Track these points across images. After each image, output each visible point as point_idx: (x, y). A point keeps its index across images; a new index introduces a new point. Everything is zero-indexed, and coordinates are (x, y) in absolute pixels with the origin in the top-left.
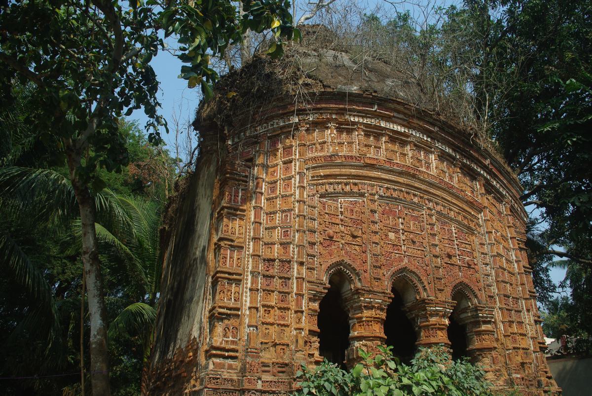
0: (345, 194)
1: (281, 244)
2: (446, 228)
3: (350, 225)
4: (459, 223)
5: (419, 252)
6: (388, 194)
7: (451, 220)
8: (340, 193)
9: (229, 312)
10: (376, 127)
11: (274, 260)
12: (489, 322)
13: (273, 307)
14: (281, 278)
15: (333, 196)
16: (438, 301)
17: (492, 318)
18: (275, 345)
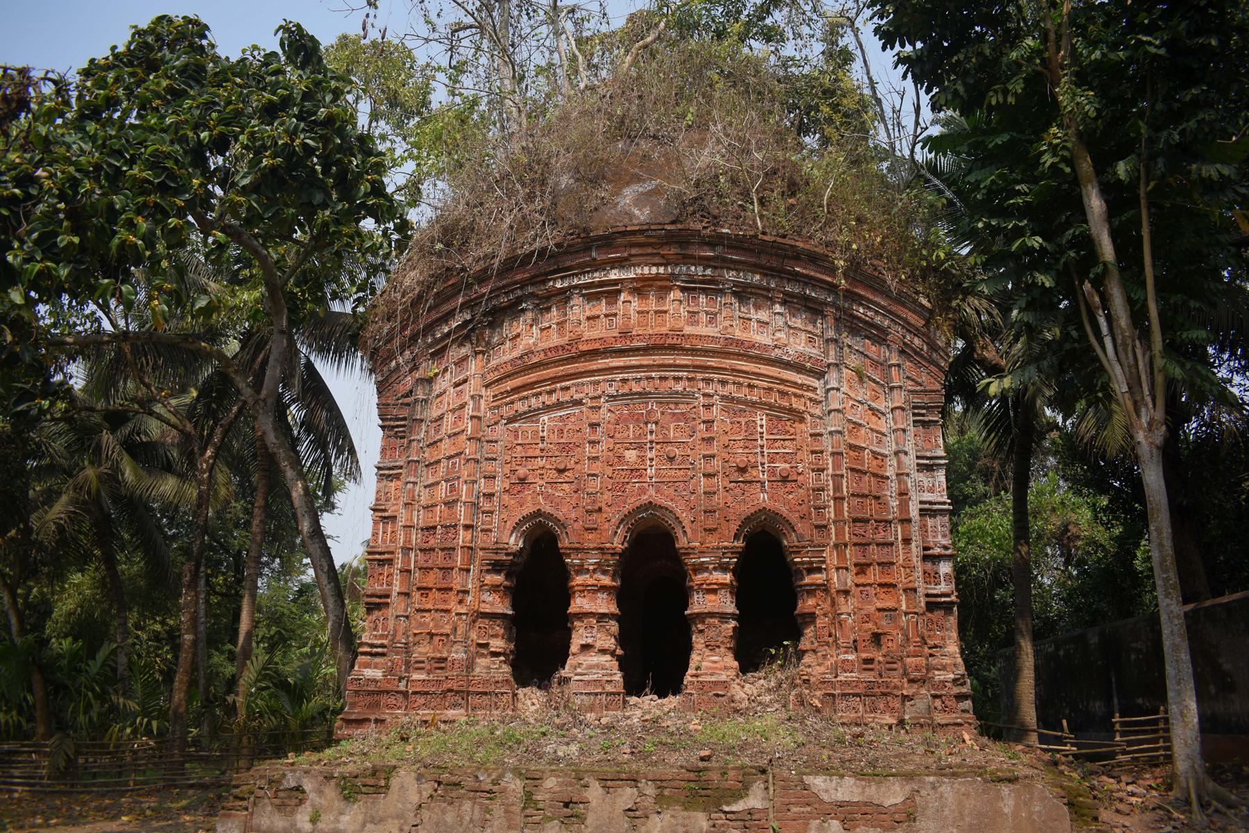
0: (548, 408)
1: (445, 504)
2: (743, 421)
3: (557, 453)
4: (771, 407)
5: (682, 472)
6: (626, 390)
7: (753, 404)
8: (539, 409)
9: (378, 600)
10: (602, 284)
11: (435, 528)
12: (819, 570)
13: (431, 589)
14: (443, 550)
15: (531, 415)
16: (593, 658)
17: (824, 562)
18: (432, 635)
